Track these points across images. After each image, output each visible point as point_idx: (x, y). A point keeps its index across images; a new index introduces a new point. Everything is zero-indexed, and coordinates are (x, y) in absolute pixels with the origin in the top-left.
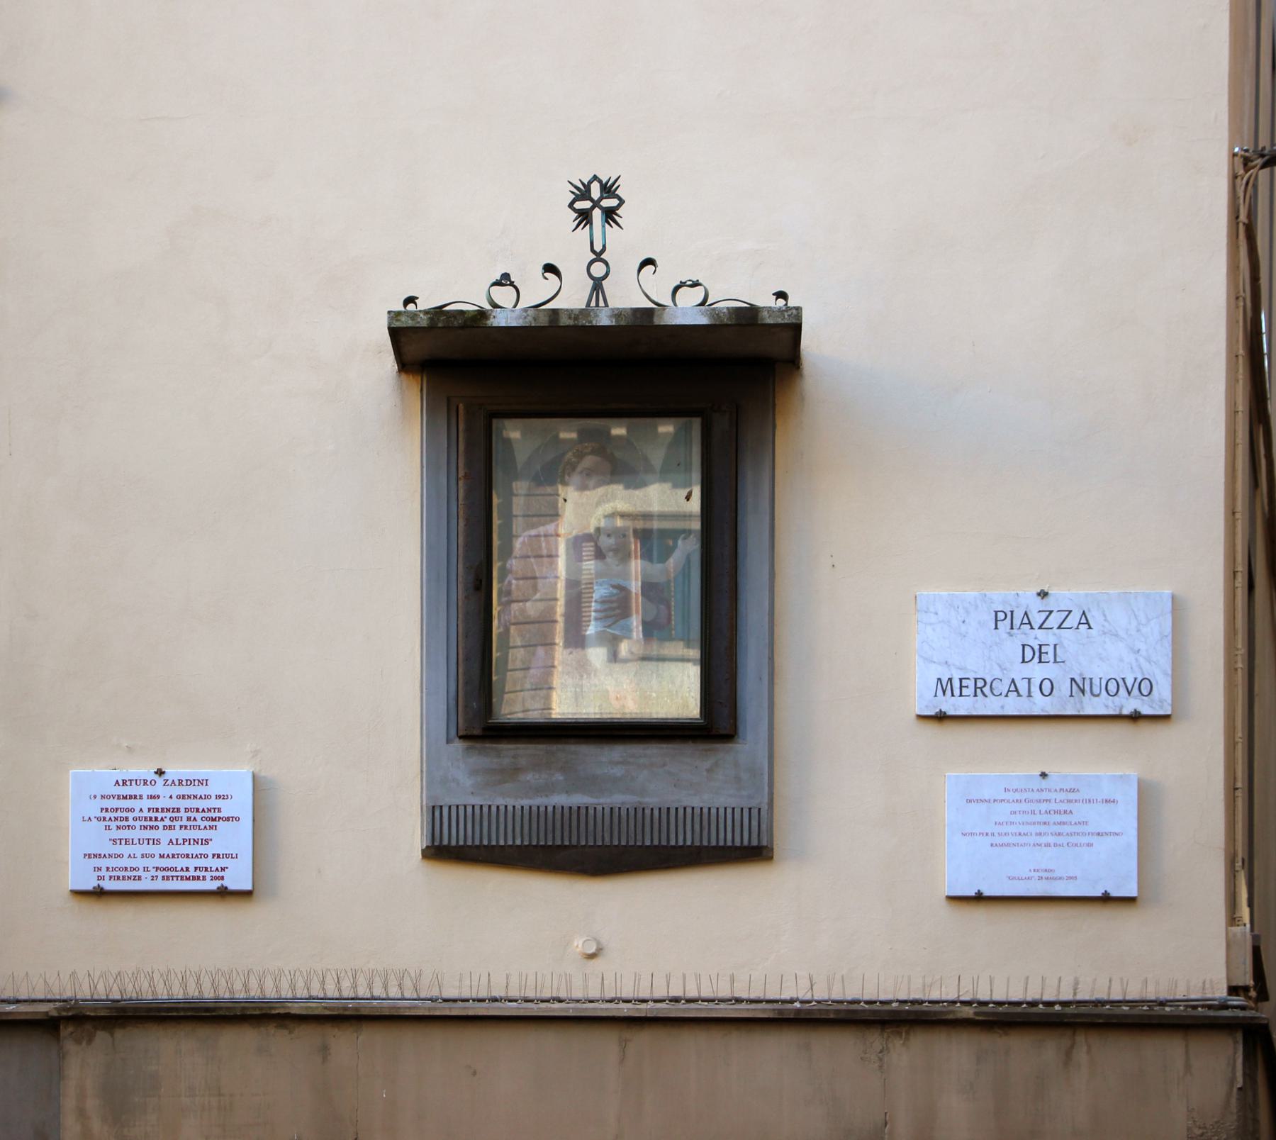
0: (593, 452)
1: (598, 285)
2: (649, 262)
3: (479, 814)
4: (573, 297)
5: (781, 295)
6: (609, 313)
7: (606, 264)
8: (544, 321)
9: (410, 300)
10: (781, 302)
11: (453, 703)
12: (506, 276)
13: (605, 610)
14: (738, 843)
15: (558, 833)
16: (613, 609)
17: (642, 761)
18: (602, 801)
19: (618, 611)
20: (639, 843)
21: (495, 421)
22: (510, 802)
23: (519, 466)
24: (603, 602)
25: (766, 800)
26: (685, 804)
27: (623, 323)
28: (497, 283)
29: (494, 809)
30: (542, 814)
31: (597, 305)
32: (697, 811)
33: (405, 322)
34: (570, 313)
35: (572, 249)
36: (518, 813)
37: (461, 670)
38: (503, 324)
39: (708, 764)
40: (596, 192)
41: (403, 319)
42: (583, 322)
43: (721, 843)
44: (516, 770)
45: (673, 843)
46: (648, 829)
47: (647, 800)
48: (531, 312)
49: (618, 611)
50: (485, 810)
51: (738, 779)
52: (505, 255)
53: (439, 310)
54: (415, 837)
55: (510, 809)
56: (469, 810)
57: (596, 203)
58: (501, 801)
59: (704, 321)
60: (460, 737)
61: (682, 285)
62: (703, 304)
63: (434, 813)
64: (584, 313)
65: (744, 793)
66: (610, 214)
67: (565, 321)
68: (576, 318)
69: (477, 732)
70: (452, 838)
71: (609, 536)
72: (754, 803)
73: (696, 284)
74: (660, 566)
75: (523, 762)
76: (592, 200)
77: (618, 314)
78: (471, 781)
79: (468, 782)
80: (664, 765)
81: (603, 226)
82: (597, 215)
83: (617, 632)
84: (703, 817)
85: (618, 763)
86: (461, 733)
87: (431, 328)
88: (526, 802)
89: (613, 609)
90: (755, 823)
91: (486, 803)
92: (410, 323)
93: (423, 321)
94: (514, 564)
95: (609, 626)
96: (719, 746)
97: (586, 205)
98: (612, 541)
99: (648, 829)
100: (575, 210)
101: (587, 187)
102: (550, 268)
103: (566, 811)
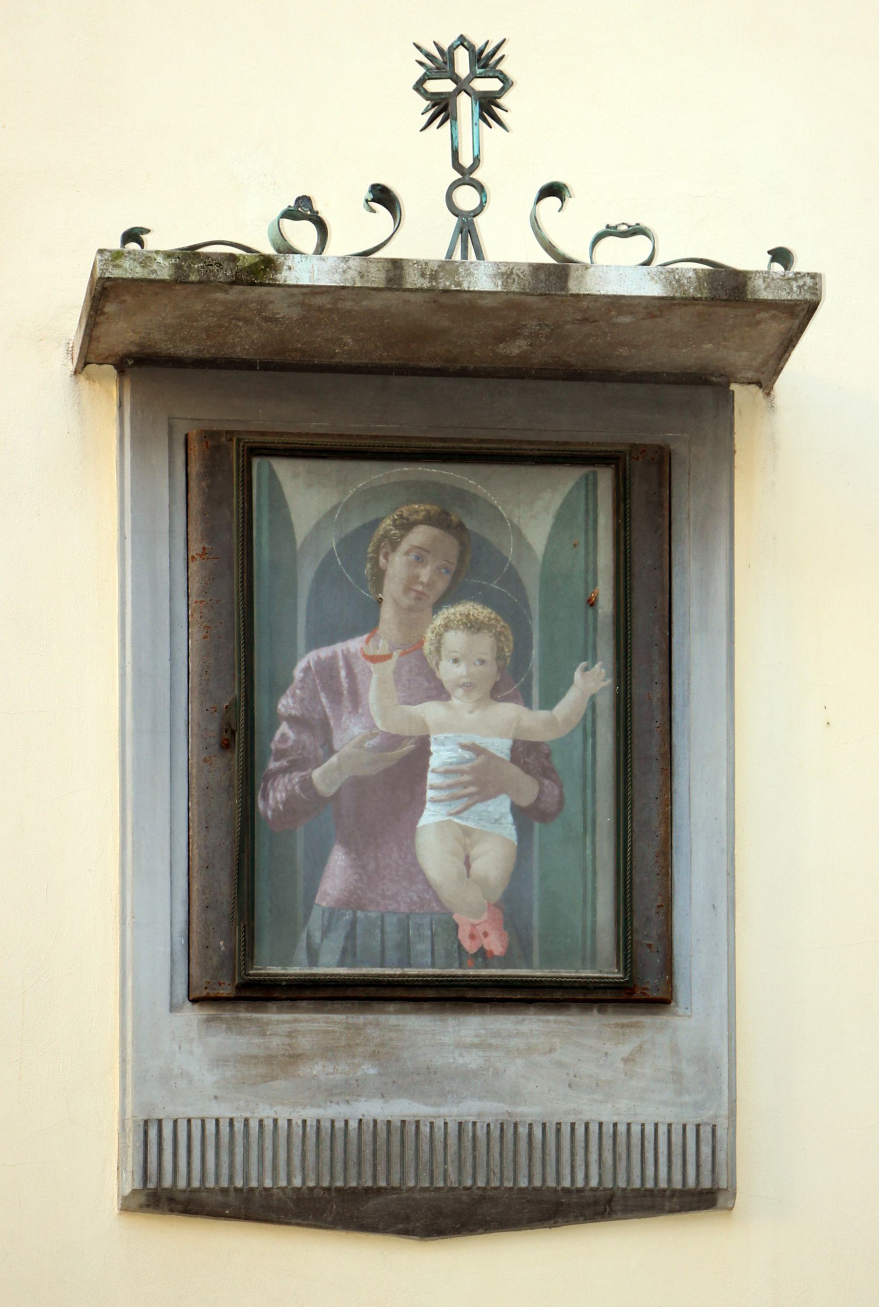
0: (429, 520)
1: (466, 229)
2: (554, 190)
3: (227, 1134)
4: (424, 239)
5: (781, 255)
6: (491, 271)
7: (480, 188)
8: (377, 278)
9: (133, 235)
10: (778, 268)
11: (181, 941)
12: (304, 200)
13: (450, 787)
14: (677, 1184)
15: (381, 1168)
16: (465, 785)
17: (513, 1043)
18: (444, 1110)
19: (472, 789)
20: (508, 1184)
21: (256, 461)
22: (283, 1113)
23: (299, 540)
24: (447, 773)
25: (725, 1112)
26: (586, 1117)
27: (515, 288)
28: (290, 214)
29: (254, 1125)
30: (340, 1135)
31: (465, 256)
32: (608, 1130)
33: (130, 269)
34: (423, 267)
35: (420, 163)
36: (298, 1131)
37: (195, 886)
38: (305, 281)
39: (625, 1049)
40: (462, 64)
41: (127, 263)
42: (445, 283)
43: (650, 1184)
44: (294, 1058)
45: (566, 1183)
46: (523, 1161)
47: (522, 1109)
48: (355, 263)
49: (472, 789)
50: (239, 1126)
51: (677, 1076)
52: (304, 163)
53: (191, 253)
54: (104, 1168)
55: (269, 1124)
56: (211, 1127)
57: (463, 84)
58: (266, 1112)
59: (654, 289)
60: (194, 1001)
61: (610, 232)
62: (647, 263)
63: (149, 1135)
64: (447, 266)
65: (686, 1098)
66: (488, 107)
67: (413, 280)
68: (434, 277)
69: (226, 991)
70: (176, 1177)
71: (456, 661)
72: (705, 1116)
73: (636, 231)
74: (544, 714)
75: (304, 1043)
76: (455, 79)
77: (507, 273)
78: (212, 1072)
79: (208, 1078)
80: (551, 1050)
81: (474, 124)
82: (465, 105)
83: (471, 824)
84: (617, 1139)
85: (473, 1046)
86: (195, 994)
87: (179, 280)
88: (311, 1113)
89: (465, 785)
90: (706, 1150)
91: (239, 1116)
92: (139, 272)
93: (164, 270)
94: (286, 704)
95: (457, 814)
96: (647, 1020)
97: (445, 86)
98: (460, 670)
99: (523, 1161)
100: (426, 95)
101: (448, 56)
102: (383, 196)
103: (382, 1129)
